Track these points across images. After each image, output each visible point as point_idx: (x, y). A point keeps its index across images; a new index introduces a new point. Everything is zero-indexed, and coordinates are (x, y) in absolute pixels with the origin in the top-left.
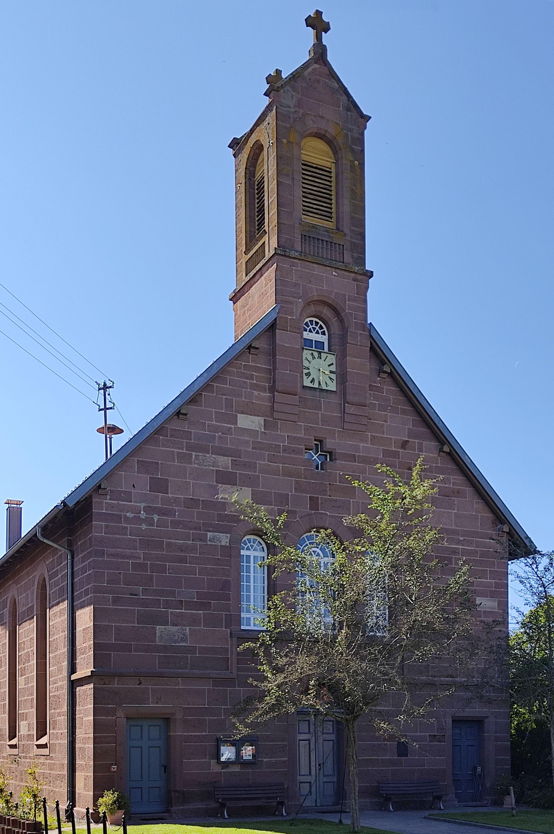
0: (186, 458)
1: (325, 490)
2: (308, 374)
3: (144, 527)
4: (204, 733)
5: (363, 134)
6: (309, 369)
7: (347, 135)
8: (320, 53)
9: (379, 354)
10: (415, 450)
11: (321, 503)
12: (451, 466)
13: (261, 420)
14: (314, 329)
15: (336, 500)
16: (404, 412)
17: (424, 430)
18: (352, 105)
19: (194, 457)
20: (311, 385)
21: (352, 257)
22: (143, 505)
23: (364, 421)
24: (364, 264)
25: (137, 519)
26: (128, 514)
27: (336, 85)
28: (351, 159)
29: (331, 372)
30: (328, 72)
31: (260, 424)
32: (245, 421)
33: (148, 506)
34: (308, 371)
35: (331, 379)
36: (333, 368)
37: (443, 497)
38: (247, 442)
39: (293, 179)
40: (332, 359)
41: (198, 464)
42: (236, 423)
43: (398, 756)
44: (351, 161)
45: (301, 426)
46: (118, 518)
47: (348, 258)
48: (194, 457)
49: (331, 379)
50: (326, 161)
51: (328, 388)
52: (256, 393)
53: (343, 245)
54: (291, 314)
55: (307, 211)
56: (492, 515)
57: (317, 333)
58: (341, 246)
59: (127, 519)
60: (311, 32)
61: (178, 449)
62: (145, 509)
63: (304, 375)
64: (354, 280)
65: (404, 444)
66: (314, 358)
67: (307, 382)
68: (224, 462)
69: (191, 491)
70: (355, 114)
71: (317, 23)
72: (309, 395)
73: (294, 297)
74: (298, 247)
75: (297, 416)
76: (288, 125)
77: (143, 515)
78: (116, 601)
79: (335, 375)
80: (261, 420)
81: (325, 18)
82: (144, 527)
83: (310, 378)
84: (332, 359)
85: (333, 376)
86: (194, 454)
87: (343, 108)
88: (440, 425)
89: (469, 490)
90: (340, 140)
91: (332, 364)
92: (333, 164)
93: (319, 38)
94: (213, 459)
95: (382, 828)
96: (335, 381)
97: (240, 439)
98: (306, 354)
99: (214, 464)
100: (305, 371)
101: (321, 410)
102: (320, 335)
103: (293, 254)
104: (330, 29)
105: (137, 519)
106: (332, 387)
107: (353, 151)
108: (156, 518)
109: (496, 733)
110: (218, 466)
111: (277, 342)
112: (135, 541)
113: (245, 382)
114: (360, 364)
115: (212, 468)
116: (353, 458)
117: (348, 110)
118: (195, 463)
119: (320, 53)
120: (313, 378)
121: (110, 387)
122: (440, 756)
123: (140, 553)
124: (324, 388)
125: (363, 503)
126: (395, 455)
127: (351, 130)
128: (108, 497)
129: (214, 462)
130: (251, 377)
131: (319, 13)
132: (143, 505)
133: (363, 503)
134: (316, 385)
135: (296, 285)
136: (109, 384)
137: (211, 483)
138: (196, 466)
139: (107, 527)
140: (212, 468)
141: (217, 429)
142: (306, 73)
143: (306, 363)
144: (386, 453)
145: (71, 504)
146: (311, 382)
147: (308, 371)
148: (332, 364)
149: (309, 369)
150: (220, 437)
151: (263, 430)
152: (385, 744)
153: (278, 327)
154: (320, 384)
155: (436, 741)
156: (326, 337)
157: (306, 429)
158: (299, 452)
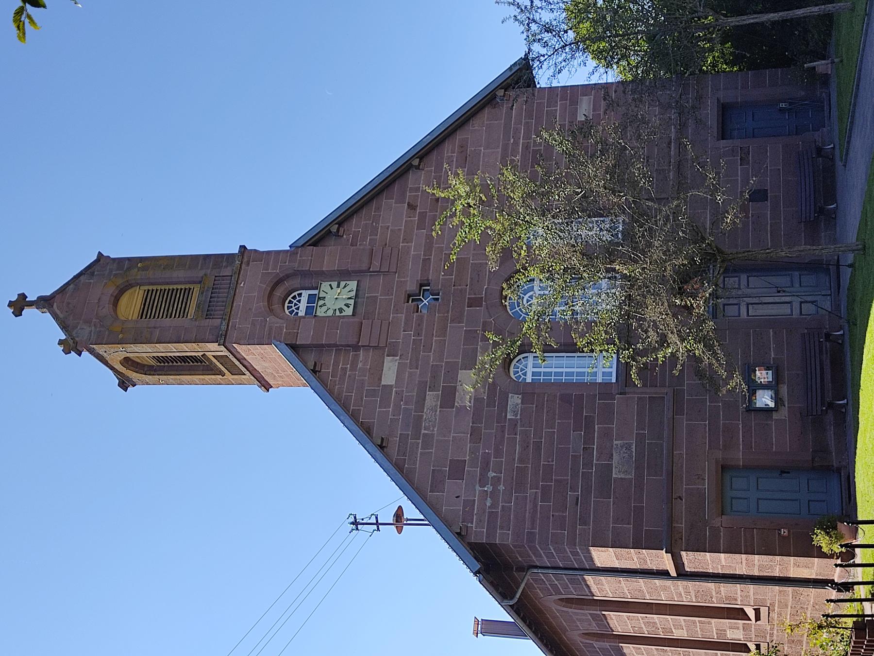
2: (341, 310)
3: (501, 487)
7: (115, 275)
8: (44, 303)
9: (320, 237)
12: (434, 155)
13: (387, 359)
15: (472, 279)
16: (378, 209)
17: (396, 186)
20: (352, 307)
21: (226, 267)
22: (478, 488)
23: (388, 250)
27: (72, 286)
28: (136, 270)
31: (392, 361)
32: (389, 377)
38: (410, 374)
40: (325, 286)
41: (434, 427)
42: (391, 386)
46: (492, 516)
51: (355, 289)
52: (360, 365)
55: (184, 313)
57: (299, 301)
60: (27, 311)
61: (418, 448)
64: (248, 264)
65: (412, 207)
66: (324, 305)
67: (349, 311)
68: (432, 399)
71: (19, 305)
72: (361, 310)
73: (265, 326)
77: (488, 488)
78: (584, 522)
80: (387, 359)
81: (14, 298)
82: (501, 487)
83: (345, 308)
84: (325, 286)
85: (343, 284)
86: (423, 431)
89: (459, 136)
90: (120, 281)
93: (31, 304)
100: (338, 313)
101: (377, 297)
102: (302, 298)
103: (224, 327)
105: (494, 494)
106: (353, 285)
107: (129, 269)
108: (491, 474)
109: (737, 88)
113: (349, 376)
114: (330, 256)
116: (426, 261)
117: (92, 274)
119: (44, 303)
123: (530, 492)
126: (422, 216)
128: (469, 525)
130: (344, 370)
131: (11, 304)
134: (352, 302)
136: (352, 519)
139: (502, 528)
141: (397, 407)
142: (61, 316)
143: (330, 313)
145: (478, 566)
150: (406, 404)
156: (303, 292)
157: (396, 311)
158: (420, 319)
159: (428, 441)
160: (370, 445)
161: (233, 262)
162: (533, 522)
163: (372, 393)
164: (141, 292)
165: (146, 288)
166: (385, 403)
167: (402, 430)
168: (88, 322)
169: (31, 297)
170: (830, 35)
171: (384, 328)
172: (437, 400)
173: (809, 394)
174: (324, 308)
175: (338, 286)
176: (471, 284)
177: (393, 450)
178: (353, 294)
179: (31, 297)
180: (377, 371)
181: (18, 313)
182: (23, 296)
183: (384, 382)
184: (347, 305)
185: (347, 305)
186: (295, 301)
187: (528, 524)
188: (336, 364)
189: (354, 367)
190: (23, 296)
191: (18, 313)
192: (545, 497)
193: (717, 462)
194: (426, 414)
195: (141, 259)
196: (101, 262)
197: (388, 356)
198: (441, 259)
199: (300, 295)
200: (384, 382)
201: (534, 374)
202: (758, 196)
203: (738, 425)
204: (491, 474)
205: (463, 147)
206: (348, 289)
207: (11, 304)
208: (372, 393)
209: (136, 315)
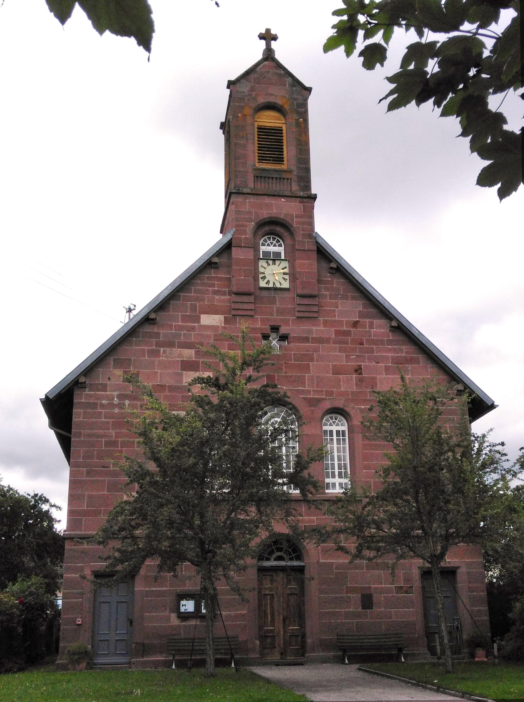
0: (157, 353)
2: (264, 278)
3: (116, 411)
4: (165, 589)
7: (293, 103)
8: (269, 54)
9: (323, 254)
10: (366, 328)
11: (278, 379)
12: (402, 338)
13: (222, 317)
15: (291, 376)
16: (353, 298)
17: (373, 310)
18: (296, 82)
19: (162, 351)
20: (267, 286)
21: (299, 185)
22: (116, 393)
23: (315, 309)
24: (310, 190)
27: (283, 72)
28: (297, 118)
29: (285, 274)
31: (220, 321)
32: (207, 320)
33: (121, 394)
35: (284, 279)
36: (287, 271)
38: (209, 336)
39: (247, 139)
40: (285, 264)
41: (165, 357)
42: (199, 322)
44: (296, 119)
45: (257, 318)
46: (94, 406)
47: (295, 187)
48: (162, 351)
49: (284, 279)
50: (275, 123)
51: (282, 287)
52: (217, 297)
55: (261, 159)
56: (445, 377)
57: (275, 245)
59: (102, 406)
60: (263, 42)
61: (148, 346)
62: (119, 396)
63: (260, 279)
64: (300, 202)
65: (355, 324)
68: (189, 354)
69: (159, 379)
70: (299, 88)
71: (268, 37)
72: (265, 293)
76: (243, 104)
77: (116, 401)
78: (88, 473)
79: (288, 276)
80: (222, 317)
83: (266, 280)
85: (287, 277)
86: (162, 349)
88: (386, 305)
89: (421, 357)
90: (287, 107)
91: (286, 267)
93: (268, 45)
94: (178, 352)
95: (400, 699)
96: (288, 281)
97: (202, 334)
99: (180, 355)
100: (261, 276)
101: (276, 304)
102: (277, 247)
104: (363, 66)
105: (112, 406)
106: (286, 285)
107: (298, 113)
108: (127, 402)
109: (470, 583)
110: (183, 357)
113: (207, 290)
114: (310, 265)
116: (306, 340)
117: (293, 86)
118: (163, 356)
119: (269, 54)
123: (113, 432)
126: (347, 333)
127: (295, 99)
130: (213, 285)
131: (268, 31)
132: (116, 393)
133: (317, 377)
134: (271, 285)
137: (176, 371)
138: (163, 358)
139: (85, 413)
140: (177, 359)
141: (181, 328)
142: (258, 69)
144: (337, 333)
145: (51, 397)
146: (266, 283)
148: (286, 267)
150: (185, 335)
152: (348, 597)
153: (233, 245)
154: (274, 284)
156: (283, 248)
157: (263, 320)
158: (256, 339)
159: (155, 353)
161: (303, 190)
162: (90, 436)
163: (193, 308)
164: (280, 125)
165: (284, 128)
166: (185, 318)
167: (163, 333)
168: (252, 89)
169: (274, 45)
170: (282, 666)
171: (248, 313)
172: (187, 358)
173: (373, 637)
174: (265, 265)
178: (278, 285)
180: (212, 310)
183: (202, 316)
184: (268, 282)
185: (268, 282)
186: (275, 242)
188: (219, 279)
189: (215, 293)
190: (275, 38)
192: (108, 444)
193: (458, 568)
194: (177, 351)
195: (306, 121)
197: (225, 318)
198: (308, 351)
199: (280, 246)
200: (202, 316)
201: (331, 432)
202: (367, 601)
203: (166, 587)
207: (268, 31)
208: (193, 308)
209: (261, 124)
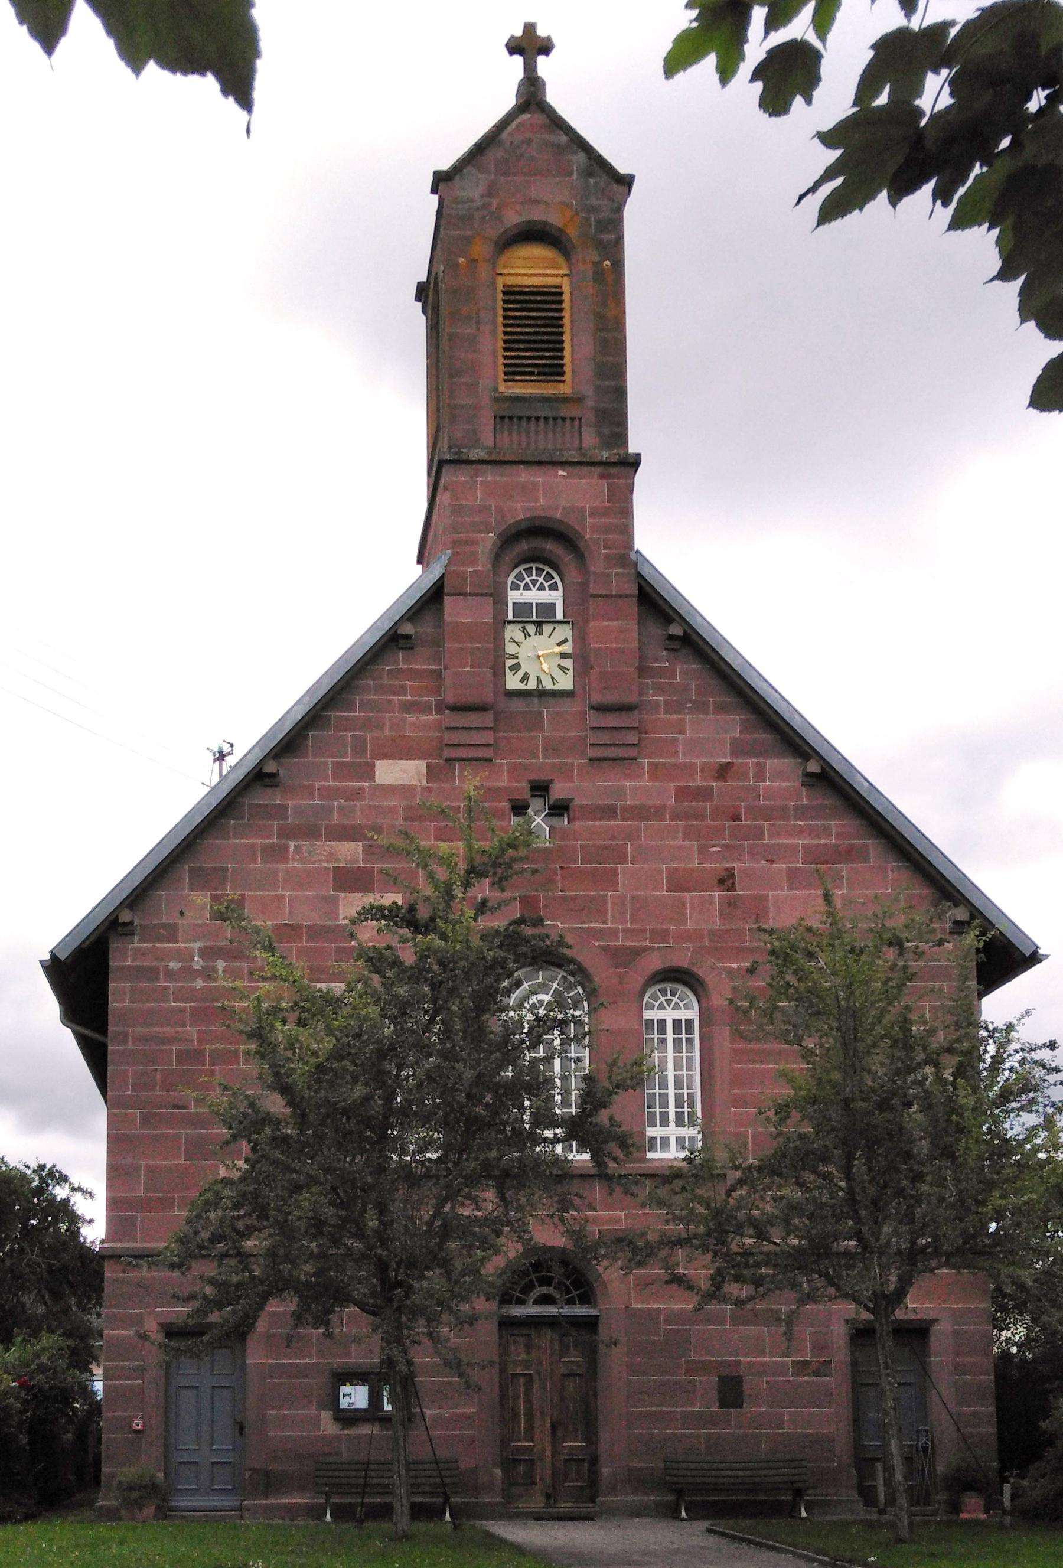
1: (552, 881)
2: (516, 668)
3: (199, 984)
4: (307, 1361)
5: (619, 209)
6: (517, 658)
7: (587, 219)
8: (531, 93)
10: (747, 779)
11: (545, 906)
12: (830, 800)
14: (534, 582)
16: (721, 708)
17: (765, 737)
18: (598, 164)
19: (292, 849)
21: (600, 434)
22: (197, 945)
23: (632, 738)
24: (625, 443)
25: (189, 973)
26: (172, 965)
27: (564, 139)
28: (597, 259)
30: (547, 121)
31: (419, 773)
32: (390, 772)
33: (206, 948)
34: (515, 661)
36: (567, 648)
37: (202, 878)
38: (393, 811)
39: (478, 323)
41: (300, 861)
42: (372, 777)
43: (720, 1407)
44: (594, 263)
45: (500, 765)
46: (152, 974)
47: (589, 438)
48: (292, 849)
51: (557, 687)
52: (411, 718)
53: (580, 419)
54: (474, 561)
55: (512, 372)
57: (541, 588)
58: (577, 422)
59: (170, 974)
61: (262, 837)
63: (507, 670)
64: (602, 476)
65: (723, 772)
66: (527, 635)
67: (513, 682)
68: (351, 852)
70: (603, 180)
71: (529, 46)
72: (517, 705)
73: (480, 532)
74: (488, 439)
75: (446, 742)
77: (198, 962)
78: (146, 1120)
81: (541, 32)
82: (199, 984)
83: (520, 674)
84: (565, 632)
85: (568, 663)
86: (292, 844)
87: (578, 173)
88: (796, 724)
89: (873, 846)
90: (573, 232)
91: (566, 640)
92: (565, 278)
93: (530, 69)
94: (328, 849)
96: (571, 673)
98: (512, 632)
99: (331, 856)
100: (509, 663)
101: (542, 729)
102: (547, 592)
103: (475, 454)
105: (189, 973)
106: (566, 682)
108: (221, 965)
109: (958, 1354)
111: (446, 617)
112: (182, 1010)
113: (389, 701)
114: (621, 631)
115: (326, 865)
116: (610, 812)
117: (590, 174)
118: (294, 860)
119: (531, 93)
120: (526, 674)
121: (229, 754)
122: (818, 1407)
123: (192, 1031)
124: (548, 688)
125: (633, 897)
126: (704, 793)
127: (594, 209)
128: (136, 938)
129: (331, 854)
130: (402, 690)
131: (530, 28)
132: (197, 945)
133: (633, 897)
134: (532, 685)
135: (483, 509)
136: (226, 749)
138: (296, 864)
139: (133, 990)
140: (326, 865)
141: (330, 794)
142: (504, 135)
143: (510, 648)
144: (682, 793)
145: (62, 956)
146: (522, 681)
147: (515, 661)
148: (566, 640)
149: (517, 658)
151: (425, 783)
152: (690, 1382)
153: (445, 591)
155: (808, 1375)
157: (513, 770)
159: (277, 853)
160: (259, 755)
161: (609, 446)
162: (145, 1039)
163: (359, 746)
164: (556, 281)
166: (342, 771)
168: (491, 191)
169: (544, 65)
175: (563, 655)
176: (564, 899)
177: (260, 797)
178: (548, 685)
179: (544, 65)
181: (514, 47)
182: (545, 48)
183: (379, 764)
184: (525, 678)
187: (140, 1030)
188: (415, 674)
189: (409, 707)
190: (545, 48)
191: (514, 47)
194: (324, 846)
195: (618, 265)
196: (615, 186)
197: (429, 766)
200: (379, 764)
201: (662, 1023)
204: (221, 965)
205: (848, 855)
206: (558, 674)
207: (530, 28)
